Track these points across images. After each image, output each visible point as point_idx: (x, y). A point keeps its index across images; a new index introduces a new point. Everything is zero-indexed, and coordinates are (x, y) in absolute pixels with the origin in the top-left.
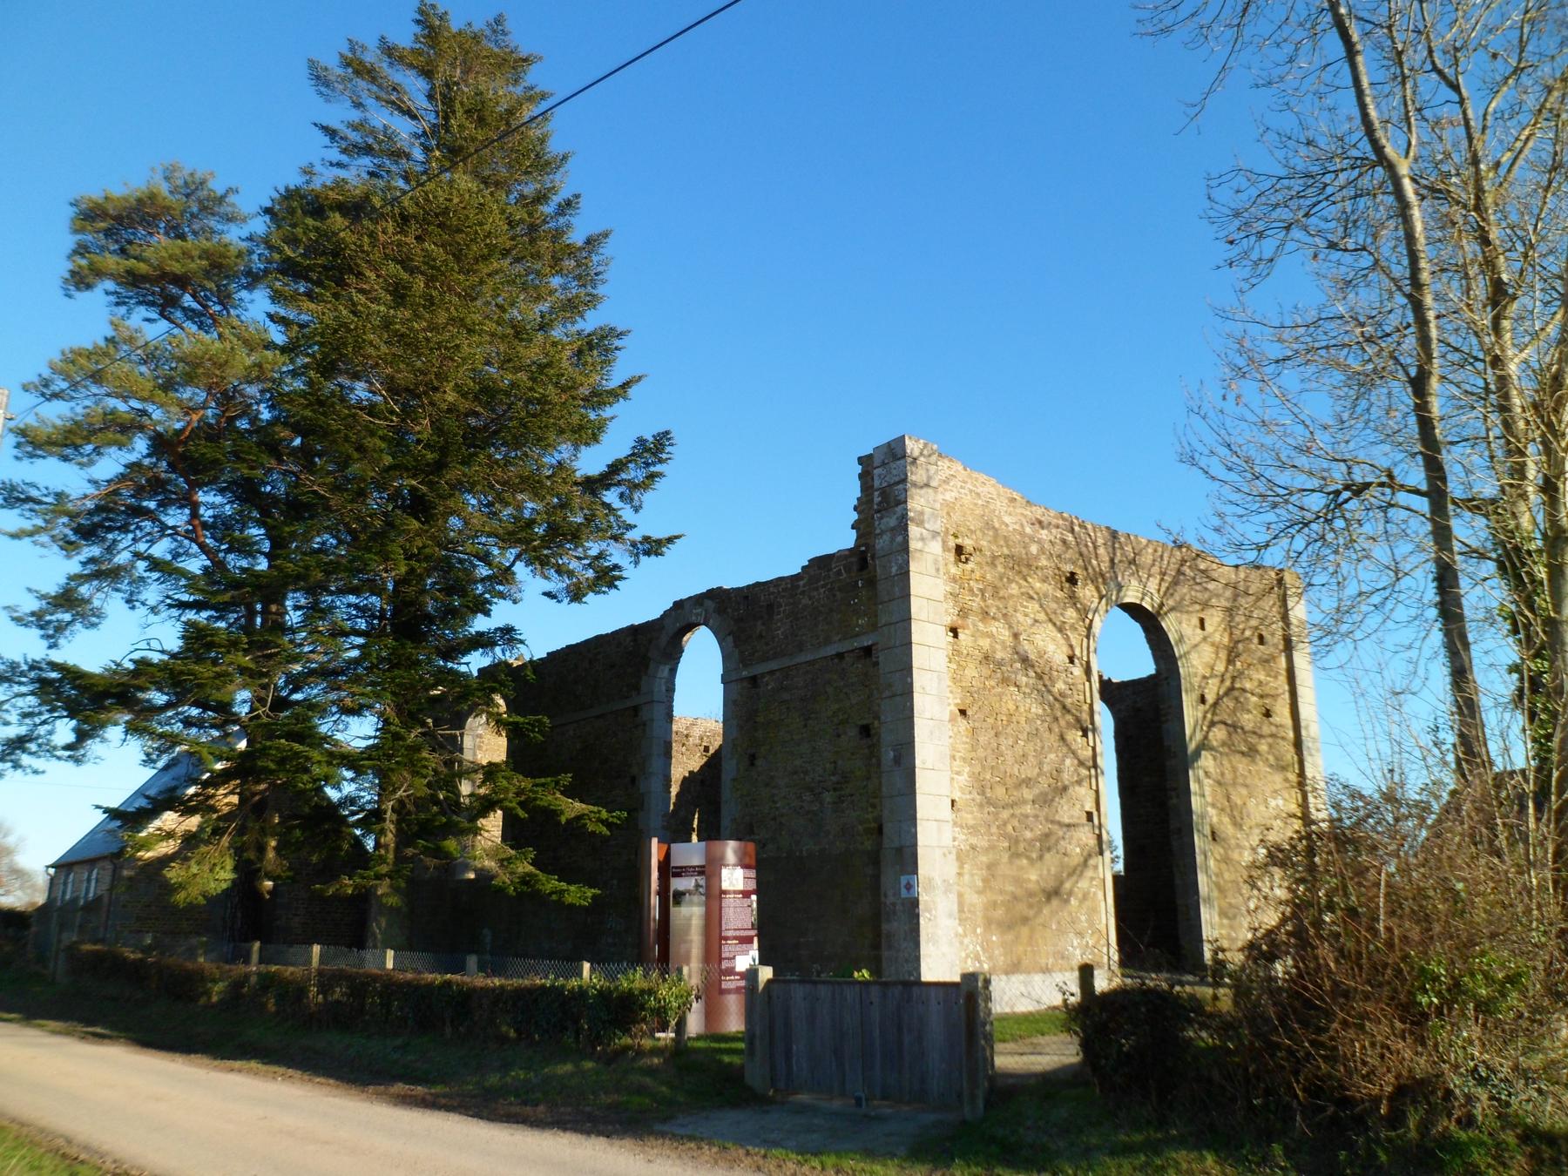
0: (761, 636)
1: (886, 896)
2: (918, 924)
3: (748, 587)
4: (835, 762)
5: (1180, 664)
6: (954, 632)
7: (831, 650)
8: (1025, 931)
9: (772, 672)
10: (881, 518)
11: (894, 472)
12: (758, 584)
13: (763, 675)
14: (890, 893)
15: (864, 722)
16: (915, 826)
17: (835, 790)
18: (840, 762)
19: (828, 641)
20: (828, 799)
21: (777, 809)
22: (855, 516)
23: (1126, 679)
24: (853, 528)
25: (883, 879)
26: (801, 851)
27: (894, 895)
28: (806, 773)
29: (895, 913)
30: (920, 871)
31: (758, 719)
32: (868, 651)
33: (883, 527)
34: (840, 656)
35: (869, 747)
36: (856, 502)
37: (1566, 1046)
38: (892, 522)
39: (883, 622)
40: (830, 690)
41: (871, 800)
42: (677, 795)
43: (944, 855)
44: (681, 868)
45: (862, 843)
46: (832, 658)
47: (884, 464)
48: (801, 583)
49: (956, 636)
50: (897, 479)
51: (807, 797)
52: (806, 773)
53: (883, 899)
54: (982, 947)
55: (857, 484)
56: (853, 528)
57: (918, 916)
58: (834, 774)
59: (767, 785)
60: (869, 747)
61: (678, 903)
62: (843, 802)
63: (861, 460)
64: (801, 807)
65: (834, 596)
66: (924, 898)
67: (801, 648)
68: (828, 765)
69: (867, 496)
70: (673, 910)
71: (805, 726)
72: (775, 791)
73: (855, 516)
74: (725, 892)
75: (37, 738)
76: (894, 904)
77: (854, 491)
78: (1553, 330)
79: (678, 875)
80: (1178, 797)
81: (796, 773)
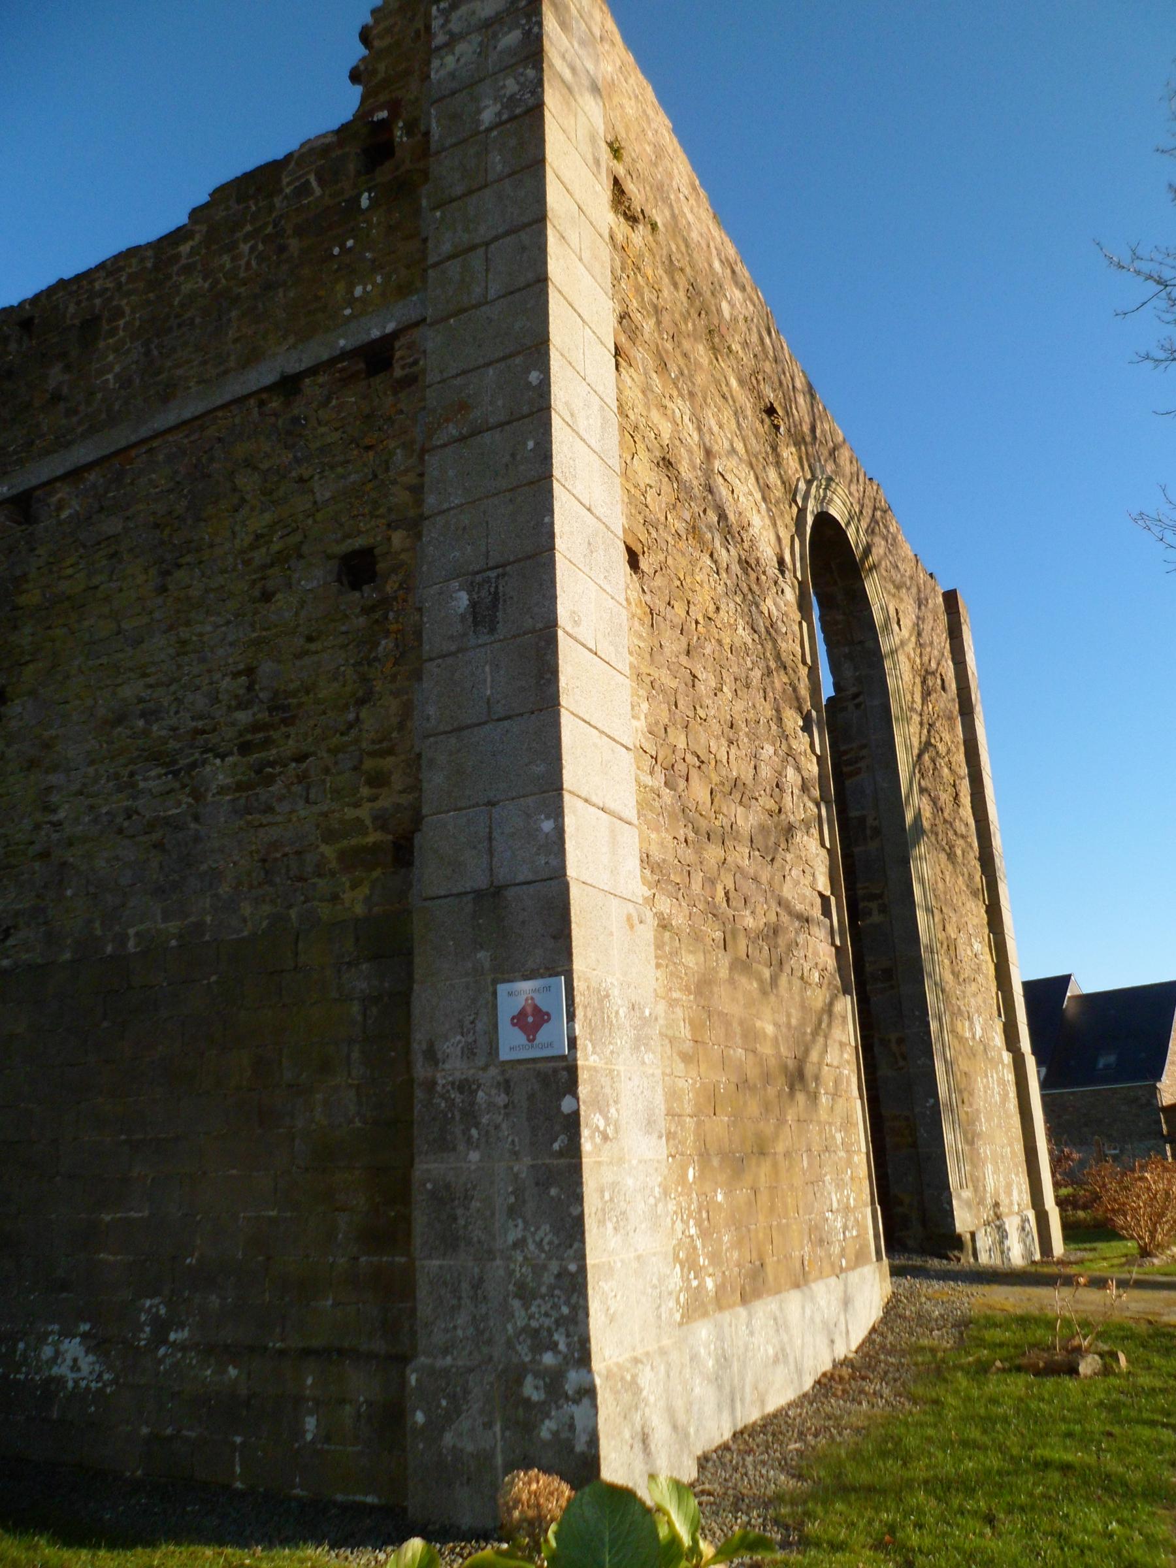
0: (56, 398)
1: (431, 1056)
2: (574, 1150)
3: (36, 299)
4: (250, 671)
5: (888, 664)
7: (264, 375)
8: (763, 1171)
9: (74, 475)
12: (61, 284)
14: (451, 1047)
16: (557, 813)
17: (245, 748)
18: (267, 667)
19: (252, 357)
20: (222, 779)
21: (57, 825)
22: (369, 20)
25: (422, 998)
26: (122, 939)
27: (469, 1052)
28: (152, 714)
29: (470, 1116)
30: (580, 964)
31: (22, 600)
33: (455, 26)
34: (289, 385)
35: (367, 610)
39: (447, 248)
40: (247, 482)
41: (369, 764)
45: (335, 898)
46: (262, 395)
48: (185, 248)
51: (153, 780)
52: (152, 714)
53: (421, 1071)
54: (699, 1224)
57: (572, 1124)
58: (242, 706)
59: (32, 764)
60: (367, 610)
62: (270, 780)
64: (129, 814)
65: (282, 249)
66: (588, 1060)
67: (167, 395)
68: (226, 683)
71: (163, 589)
72: (54, 779)
73: (369, 20)
76: (466, 1087)
80: (883, 909)
81: (120, 719)
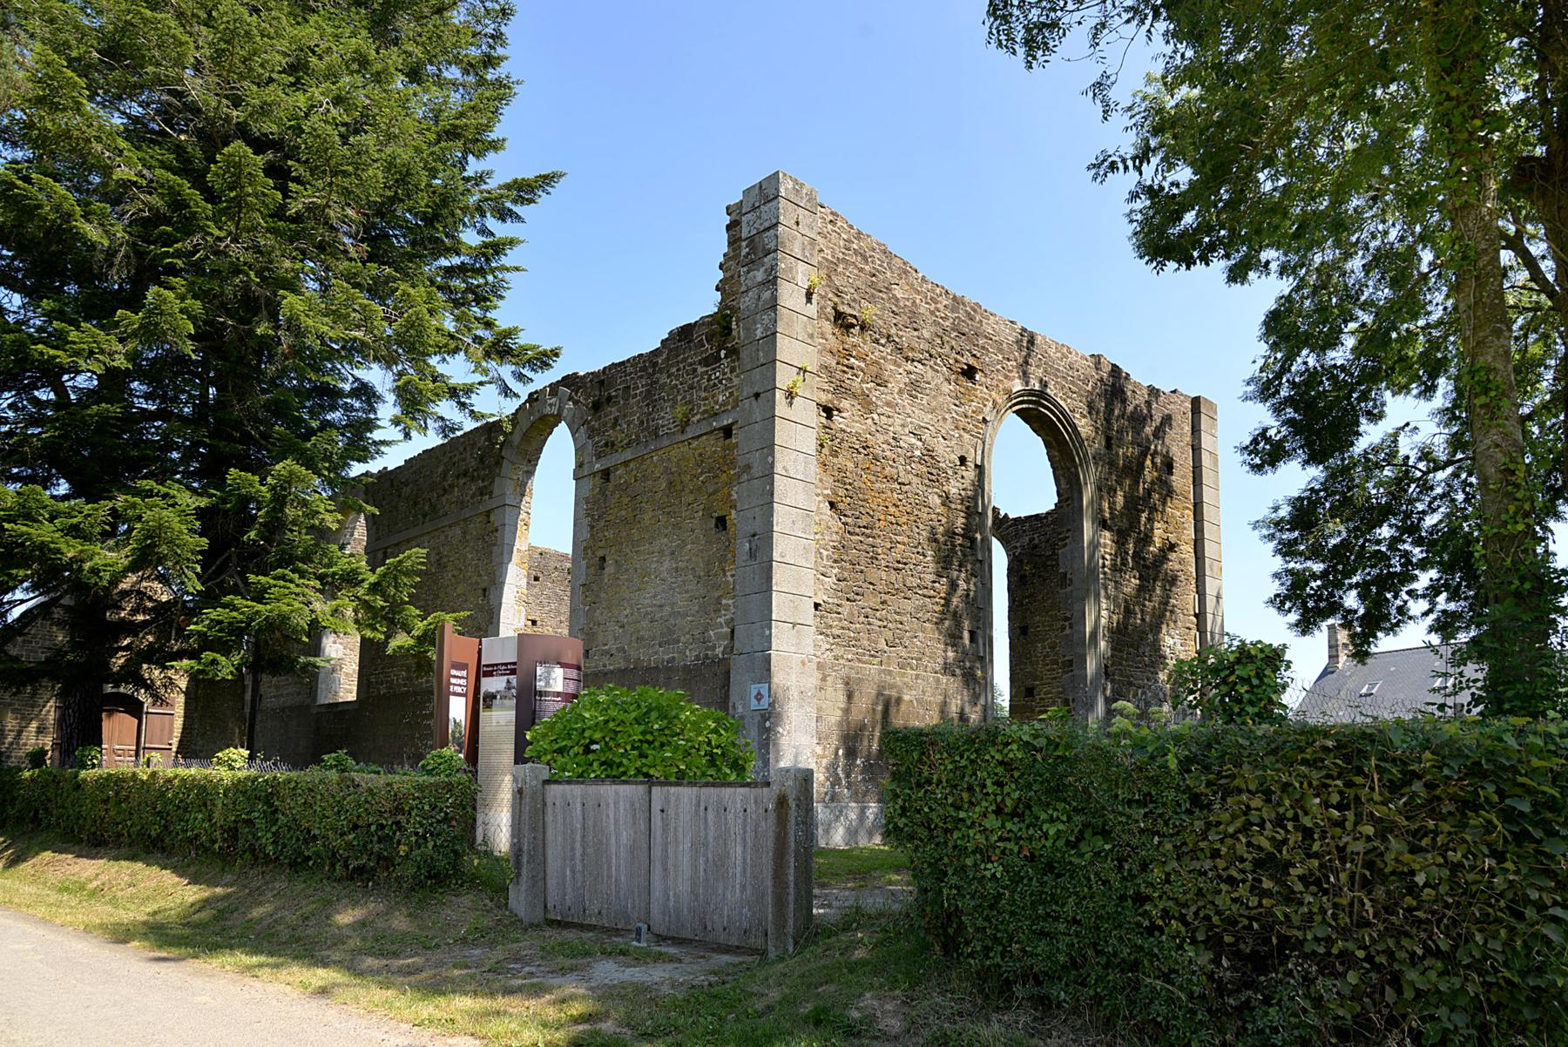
6: (828, 411)
9: (626, 463)
10: (748, 272)
11: (764, 216)
13: (616, 467)
15: (721, 513)
23: (1023, 514)
24: (717, 289)
32: (727, 431)
36: (722, 259)
37: (1561, 886)
38: (760, 275)
42: (384, 473)
43: (803, 663)
44: (492, 665)
47: (754, 209)
49: (829, 417)
50: (767, 225)
55: (724, 237)
56: (717, 289)
61: (488, 707)
63: (729, 210)
69: (734, 250)
70: (483, 715)
74: (541, 694)
75: (25, 635)
77: (721, 245)
78: (1289, 583)
79: (489, 674)
